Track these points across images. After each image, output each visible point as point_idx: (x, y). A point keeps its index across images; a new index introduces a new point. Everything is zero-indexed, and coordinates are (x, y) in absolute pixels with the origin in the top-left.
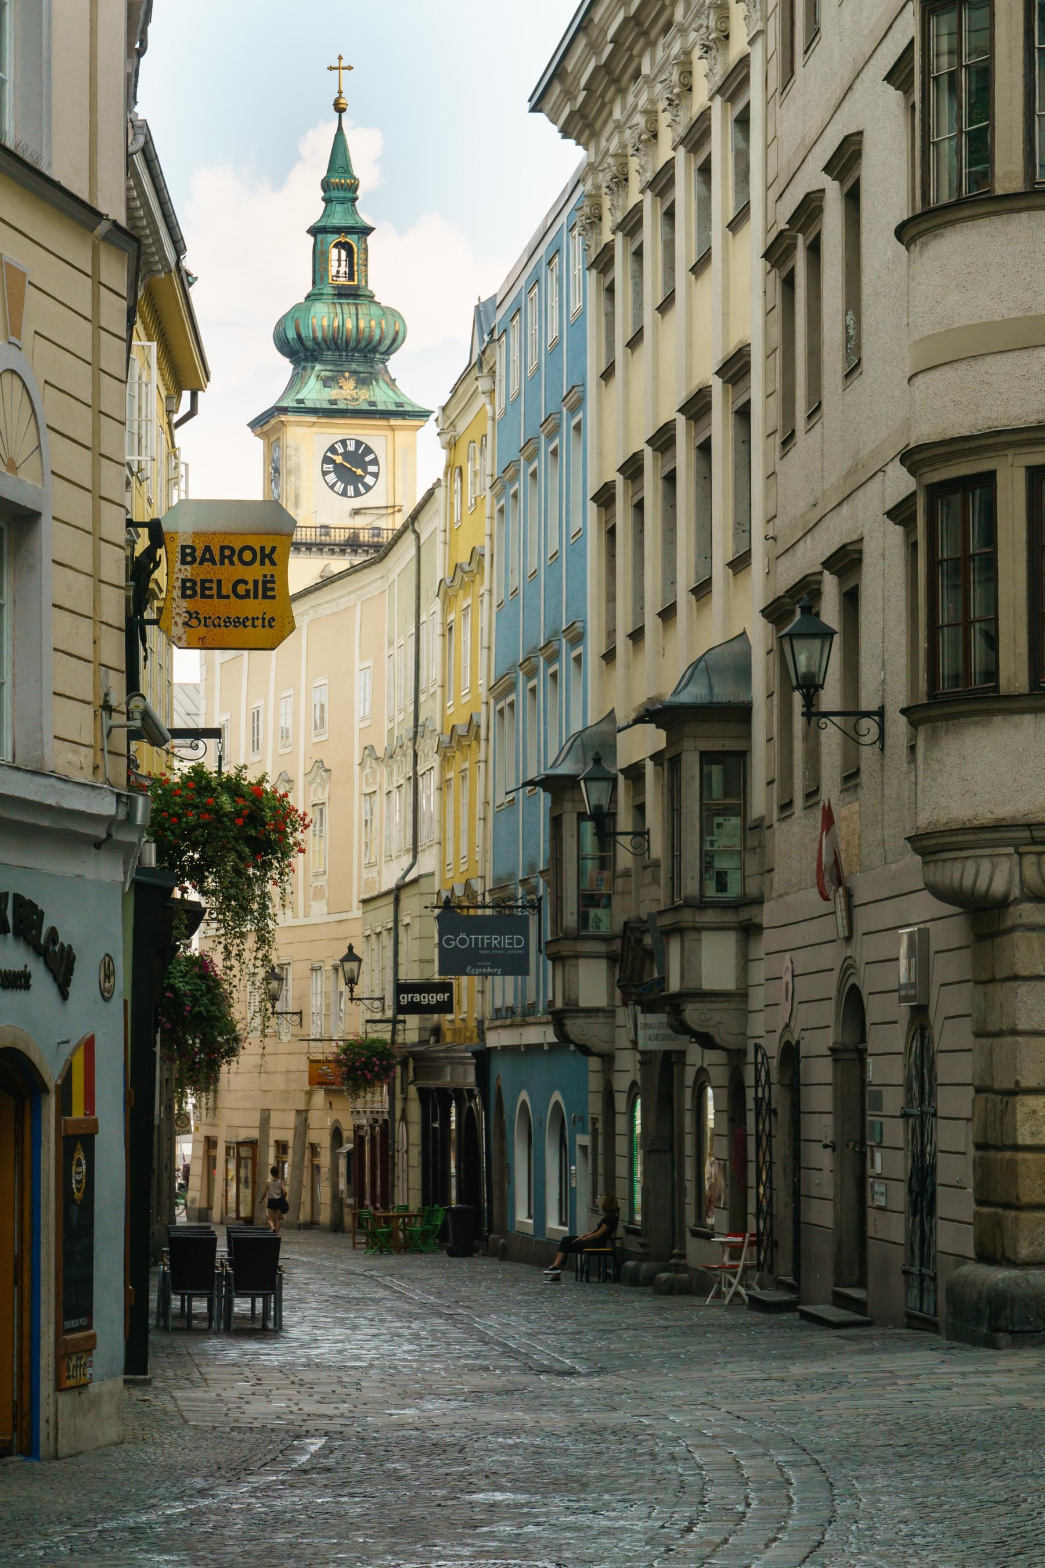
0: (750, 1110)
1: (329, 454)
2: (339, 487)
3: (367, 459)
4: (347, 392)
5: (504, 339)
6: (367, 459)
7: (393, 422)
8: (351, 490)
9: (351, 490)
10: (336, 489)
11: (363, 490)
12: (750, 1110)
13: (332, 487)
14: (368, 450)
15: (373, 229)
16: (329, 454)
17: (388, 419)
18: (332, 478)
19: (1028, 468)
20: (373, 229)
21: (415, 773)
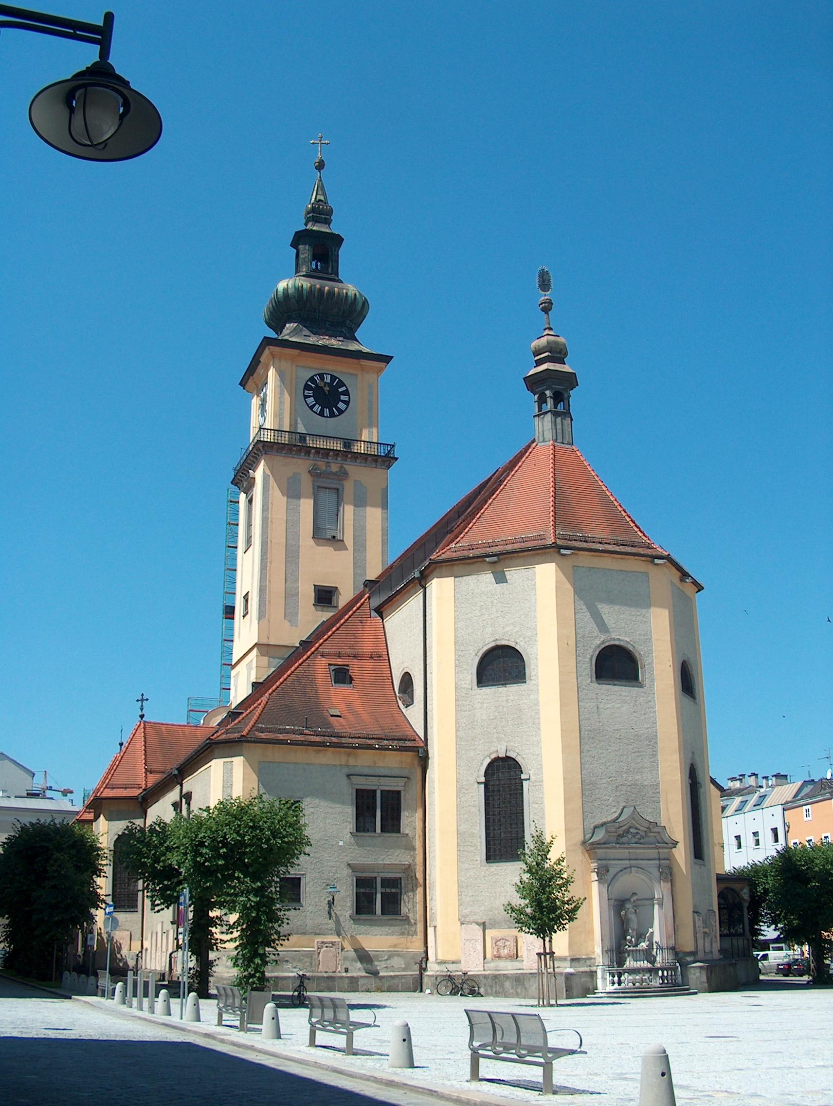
2: (317, 408)
3: (340, 390)
6: (340, 390)
8: (327, 412)
9: (327, 412)
13: (311, 408)
20: (392, 357)
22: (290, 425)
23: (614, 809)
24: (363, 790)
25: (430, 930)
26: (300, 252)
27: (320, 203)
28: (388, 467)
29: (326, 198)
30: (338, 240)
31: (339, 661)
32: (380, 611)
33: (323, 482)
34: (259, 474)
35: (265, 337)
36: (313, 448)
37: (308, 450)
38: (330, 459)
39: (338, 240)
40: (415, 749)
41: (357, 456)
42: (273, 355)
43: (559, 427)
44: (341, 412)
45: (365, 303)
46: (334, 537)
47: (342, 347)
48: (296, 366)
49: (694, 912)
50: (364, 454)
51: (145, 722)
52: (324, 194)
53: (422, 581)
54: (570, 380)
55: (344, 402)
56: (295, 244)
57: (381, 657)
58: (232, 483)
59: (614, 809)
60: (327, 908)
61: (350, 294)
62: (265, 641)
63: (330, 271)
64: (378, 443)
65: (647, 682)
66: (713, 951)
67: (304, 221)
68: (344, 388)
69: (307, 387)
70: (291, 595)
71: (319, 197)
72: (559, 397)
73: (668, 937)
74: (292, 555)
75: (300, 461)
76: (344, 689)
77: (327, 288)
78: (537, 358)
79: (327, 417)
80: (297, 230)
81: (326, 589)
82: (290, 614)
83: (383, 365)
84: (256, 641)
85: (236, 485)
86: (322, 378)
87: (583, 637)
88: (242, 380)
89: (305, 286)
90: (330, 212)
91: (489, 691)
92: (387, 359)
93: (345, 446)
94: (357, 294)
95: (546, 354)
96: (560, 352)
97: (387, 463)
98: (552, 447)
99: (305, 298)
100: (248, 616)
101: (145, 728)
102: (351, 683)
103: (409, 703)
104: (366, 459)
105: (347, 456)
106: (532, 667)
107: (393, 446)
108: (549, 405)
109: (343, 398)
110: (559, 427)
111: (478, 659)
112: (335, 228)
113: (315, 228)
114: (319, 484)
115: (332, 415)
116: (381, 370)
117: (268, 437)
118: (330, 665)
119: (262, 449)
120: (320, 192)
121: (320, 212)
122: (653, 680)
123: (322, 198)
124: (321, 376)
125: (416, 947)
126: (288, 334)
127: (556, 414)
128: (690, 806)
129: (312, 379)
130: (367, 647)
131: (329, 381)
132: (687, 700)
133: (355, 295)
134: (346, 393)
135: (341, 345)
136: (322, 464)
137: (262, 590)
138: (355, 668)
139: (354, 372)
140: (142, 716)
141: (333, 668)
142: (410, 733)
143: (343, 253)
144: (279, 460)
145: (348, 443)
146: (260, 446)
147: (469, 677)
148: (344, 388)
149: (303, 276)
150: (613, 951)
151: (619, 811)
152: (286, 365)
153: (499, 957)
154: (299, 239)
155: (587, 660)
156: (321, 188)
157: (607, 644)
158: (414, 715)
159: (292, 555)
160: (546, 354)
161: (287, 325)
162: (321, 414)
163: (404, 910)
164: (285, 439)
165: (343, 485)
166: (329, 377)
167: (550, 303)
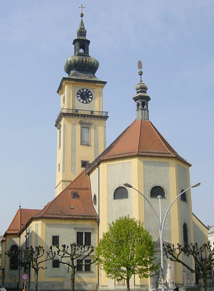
0: (90, 121)
1: (79, 92)
2: (82, 100)
3: (89, 94)
4: (83, 76)
5: (178, 285)
6: (89, 94)
7: (97, 84)
8: (85, 102)
9: (85, 102)
10: (80, 101)
11: (88, 102)
12: (90, 121)
13: (80, 100)
14: (90, 92)
15: (107, 82)
16: (79, 92)
17: (95, 83)
18: (79, 98)
19: (77, 232)
20: (107, 82)
21: (179, 261)
22: (73, 107)
23: (156, 238)
24: (79, 232)
25: (100, 276)
26: (76, 46)
27: (82, 29)
28: (106, 120)
29: (84, 27)
30: (88, 42)
31: (75, 191)
32: (89, 174)
33: (84, 126)
34: (62, 122)
35: (63, 78)
36: (80, 114)
37: (78, 115)
38: (86, 118)
39: (88, 42)
40: (96, 219)
41: (94, 117)
42: (66, 83)
43: (144, 114)
44: (90, 102)
45: (98, 64)
46: (88, 144)
47: (90, 80)
48: (74, 86)
49: (183, 271)
50: (98, 116)
51: (21, 209)
52: (83, 26)
53: (99, 164)
54: (148, 99)
55: (91, 98)
56: (74, 44)
57: (88, 189)
58: (55, 126)
59: (156, 238)
60: (41, 267)
61: (92, 61)
62: (65, 180)
63: (86, 53)
64: (102, 112)
65: (168, 198)
66: (192, 283)
67: (77, 35)
68: (91, 93)
69: (78, 94)
70: (73, 163)
71: (81, 27)
72: (143, 104)
73: (173, 279)
74: (73, 151)
75: (76, 119)
76: (76, 200)
77: (84, 59)
78: (138, 91)
79: (85, 103)
80: (74, 39)
81: (84, 161)
82: (73, 171)
83: (104, 85)
84: (62, 180)
85: (56, 127)
86: (83, 90)
87: (147, 183)
88: (58, 90)
89: (77, 59)
90: (86, 32)
91: (118, 201)
92: (105, 83)
93: (91, 113)
94: (95, 60)
95: (139, 90)
96: (145, 89)
97: (106, 118)
98: (140, 121)
99: (77, 62)
100: (60, 171)
101: (21, 211)
102: (78, 198)
103: (95, 204)
104: (98, 117)
105: (91, 117)
106: (130, 193)
107: (107, 112)
108: (140, 107)
109: (90, 96)
110: (144, 114)
111: (114, 191)
112: (87, 38)
113: (80, 38)
114: (82, 126)
115: (87, 103)
116: (103, 87)
117: (65, 111)
118: (72, 192)
119: (63, 115)
120: (82, 25)
121: (82, 32)
122: (170, 197)
123: (83, 27)
124: (83, 90)
125: (95, 280)
126: (71, 76)
127: (142, 109)
128: (183, 237)
129: (80, 91)
130: (85, 186)
131: (85, 91)
132: (183, 203)
133: (94, 61)
134: (91, 95)
135: (90, 79)
136: (83, 120)
137: (63, 163)
138: (80, 193)
139: (94, 87)
140: (20, 207)
141: (73, 193)
142: (95, 215)
143: (91, 47)
144: (70, 119)
145: (92, 112)
146: (62, 114)
147: (111, 197)
148: (91, 93)
149: (76, 55)
150: (154, 283)
151: (158, 239)
152: (71, 86)
153: (119, 285)
154: (75, 42)
155: (148, 191)
156: (82, 23)
157: (154, 186)
158: (96, 207)
159: (73, 151)
160: (139, 90)
161: (71, 72)
162: (83, 102)
163: (92, 271)
164: (71, 112)
165: (91, 126)
166: (85, 89)
167: (142, 72)
